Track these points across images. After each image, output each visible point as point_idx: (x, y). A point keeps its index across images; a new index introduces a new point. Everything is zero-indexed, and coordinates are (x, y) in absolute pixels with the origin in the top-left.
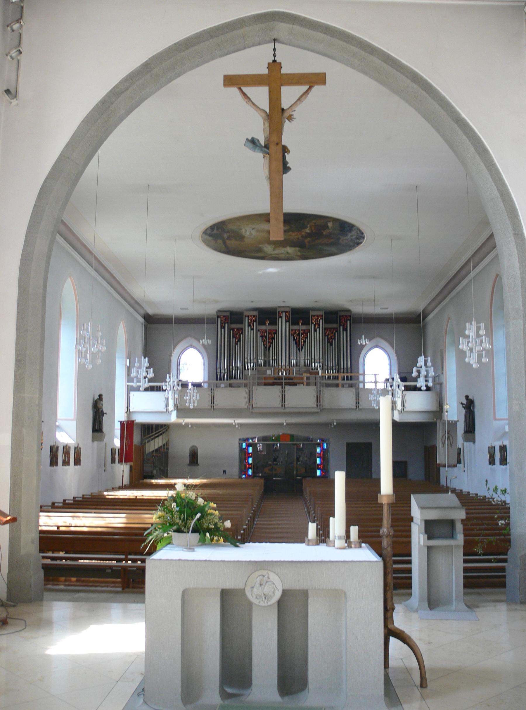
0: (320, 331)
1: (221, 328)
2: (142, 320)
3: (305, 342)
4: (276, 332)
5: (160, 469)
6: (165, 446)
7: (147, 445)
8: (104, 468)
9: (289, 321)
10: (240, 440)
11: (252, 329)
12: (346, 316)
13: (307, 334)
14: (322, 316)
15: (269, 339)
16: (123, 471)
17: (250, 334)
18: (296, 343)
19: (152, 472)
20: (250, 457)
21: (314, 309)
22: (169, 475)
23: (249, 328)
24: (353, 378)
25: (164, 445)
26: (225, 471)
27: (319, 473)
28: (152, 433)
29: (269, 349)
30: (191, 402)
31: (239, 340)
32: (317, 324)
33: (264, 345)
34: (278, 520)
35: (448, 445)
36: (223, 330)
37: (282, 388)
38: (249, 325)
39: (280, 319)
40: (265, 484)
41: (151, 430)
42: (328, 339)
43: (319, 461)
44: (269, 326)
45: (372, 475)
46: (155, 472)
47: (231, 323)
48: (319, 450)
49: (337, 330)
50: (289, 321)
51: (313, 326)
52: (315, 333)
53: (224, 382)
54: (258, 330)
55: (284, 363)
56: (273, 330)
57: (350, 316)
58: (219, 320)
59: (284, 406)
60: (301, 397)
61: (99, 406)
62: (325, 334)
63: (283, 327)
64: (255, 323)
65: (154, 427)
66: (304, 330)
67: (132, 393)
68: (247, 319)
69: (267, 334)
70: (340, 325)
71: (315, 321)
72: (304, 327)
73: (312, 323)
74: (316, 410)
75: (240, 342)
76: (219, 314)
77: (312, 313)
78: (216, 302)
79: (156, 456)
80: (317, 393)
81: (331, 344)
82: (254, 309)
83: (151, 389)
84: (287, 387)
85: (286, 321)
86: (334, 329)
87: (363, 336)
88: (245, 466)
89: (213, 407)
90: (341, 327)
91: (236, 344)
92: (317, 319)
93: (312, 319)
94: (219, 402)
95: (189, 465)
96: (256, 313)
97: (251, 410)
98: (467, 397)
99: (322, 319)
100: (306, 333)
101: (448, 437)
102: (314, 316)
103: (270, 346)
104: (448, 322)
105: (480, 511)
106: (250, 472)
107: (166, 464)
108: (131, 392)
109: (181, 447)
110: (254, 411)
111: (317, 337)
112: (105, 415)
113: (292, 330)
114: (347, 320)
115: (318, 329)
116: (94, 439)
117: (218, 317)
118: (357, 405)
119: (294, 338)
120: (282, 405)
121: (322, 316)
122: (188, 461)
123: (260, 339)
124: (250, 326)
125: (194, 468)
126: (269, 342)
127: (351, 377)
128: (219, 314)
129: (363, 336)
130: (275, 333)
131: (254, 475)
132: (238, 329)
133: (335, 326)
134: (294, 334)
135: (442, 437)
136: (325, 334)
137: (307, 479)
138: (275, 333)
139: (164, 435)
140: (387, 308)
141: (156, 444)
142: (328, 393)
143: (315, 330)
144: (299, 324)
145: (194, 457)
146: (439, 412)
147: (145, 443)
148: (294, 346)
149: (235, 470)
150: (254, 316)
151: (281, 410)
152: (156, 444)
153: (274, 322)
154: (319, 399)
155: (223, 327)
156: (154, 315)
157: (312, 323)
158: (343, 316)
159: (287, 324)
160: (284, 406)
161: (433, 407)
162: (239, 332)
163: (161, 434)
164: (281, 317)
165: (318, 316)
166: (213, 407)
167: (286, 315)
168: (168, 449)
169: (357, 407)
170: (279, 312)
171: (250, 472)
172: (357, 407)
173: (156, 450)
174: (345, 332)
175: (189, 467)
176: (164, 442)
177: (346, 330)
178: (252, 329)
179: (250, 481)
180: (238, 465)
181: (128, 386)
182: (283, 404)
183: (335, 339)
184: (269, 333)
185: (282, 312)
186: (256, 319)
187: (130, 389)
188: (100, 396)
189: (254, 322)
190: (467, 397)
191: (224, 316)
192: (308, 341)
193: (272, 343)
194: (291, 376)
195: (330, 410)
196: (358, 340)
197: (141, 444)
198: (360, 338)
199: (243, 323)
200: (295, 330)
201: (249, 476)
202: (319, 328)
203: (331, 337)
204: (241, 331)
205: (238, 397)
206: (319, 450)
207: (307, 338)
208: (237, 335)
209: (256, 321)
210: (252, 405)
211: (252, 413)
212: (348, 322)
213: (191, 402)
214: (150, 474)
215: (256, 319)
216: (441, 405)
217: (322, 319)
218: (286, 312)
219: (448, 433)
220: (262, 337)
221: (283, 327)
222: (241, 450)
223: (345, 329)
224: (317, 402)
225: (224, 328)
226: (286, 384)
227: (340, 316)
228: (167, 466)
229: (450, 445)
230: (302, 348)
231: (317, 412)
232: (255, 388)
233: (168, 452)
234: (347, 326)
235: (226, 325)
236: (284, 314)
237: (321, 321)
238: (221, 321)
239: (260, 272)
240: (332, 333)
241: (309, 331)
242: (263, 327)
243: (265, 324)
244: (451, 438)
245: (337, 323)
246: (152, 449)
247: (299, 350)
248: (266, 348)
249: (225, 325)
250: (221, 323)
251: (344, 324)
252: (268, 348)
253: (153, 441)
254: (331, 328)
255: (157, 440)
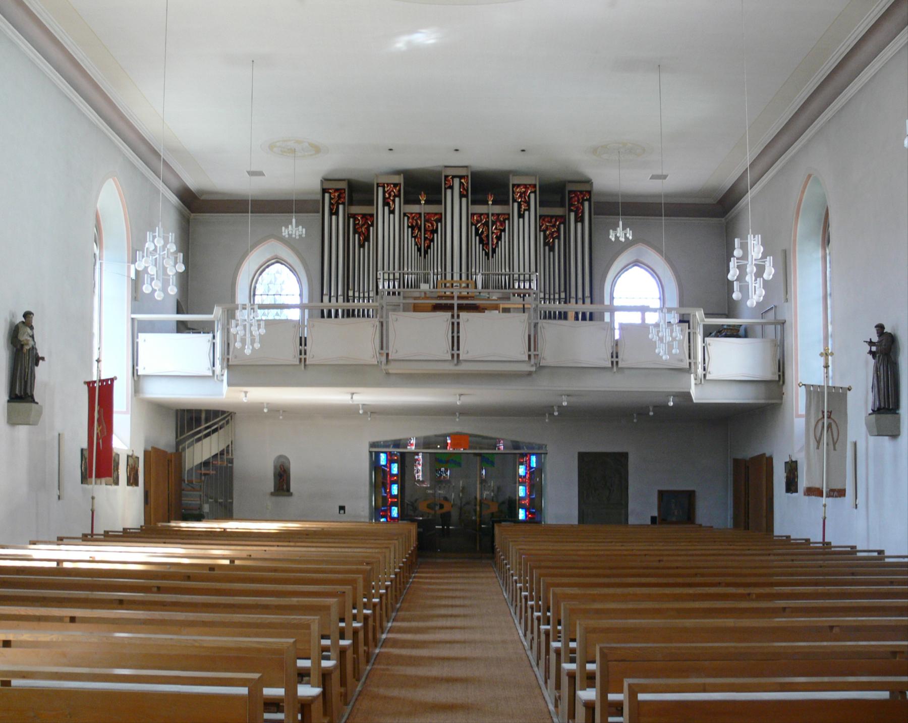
0: (531, 217)
1: (331, 214)
2: (174, 199)
3: (499, 238)
4: (440, 218)
5: (216, 502)
6: (225, 454)
7: (188, 453)
8: (56, 492)
9: (467, 196)
10: (373, 445)
11: (392, 212)
12: (581, 192)
13: (503, 223)
14: (535, 186)
15: (426, 232)
16: (124, 502)
17: (389, 226)
18: (481, 241)
19: (200, 508)
20: (395, 482)
21: (515, 173)
22: (234, 516)
23: (386, 208)
24: (595, 316)
25: (222, 453)
26: (342, 508)
27: (522, 514)
28: (200, 426)
29: (426, 252)
30: (248, 340)
31: (367, 239)
32: (525, 202)
33: (416, 244)
34: (456, 590)
35: (828, 444)
36: (334, 217)
37: (453, 316)
38: (386, 203)
39: (449, 192)
40: (420, 536)
41: (192, 421)
42: (545, 237)
43: (522, 491)
44: (426, 206)
45: (627, 520)
46: (206, 508)
47: (351, 203)
48: (522, 470)
49: (563, 219)
50: (467, 196)
51: (516, 205)
52: (521, 220)
53: (337, 320)
54: (405, 215)
55: (456, 277)
56: (436, 214)
57: (589, 192)
58: (327, 195)
59: (456, 358)
60: (495, 336)
61: (23, 337)
62: (540, 228)
63: (456, 210)
64: (397, 200)
65: (203, 416)
66: (498, 215)
67: (142, 337)
68: (380, 189)
69: (422, 222)
70: (570, 211)
71: (520, 196)
72: (497, 209)
73: (514, 200)
74: (526, 368)
75: (369, 241)
76: (326, 186)
77: (514, 180)
78: (317, 149)
79: (205, 475)
80: (529, 330)
81: (552, 249)
82: (398, 172)
83: (183, 327)
84: (464, 315)
85: (462, 196)
86: (557, 217)
87: (621, 223)
88: (384, 499)
89: (303, 361)
90: (572, 215)
91: (362, 246)
92: (525, 193)
93: (513, 192)
94: (317, 352)
95: (272, 494)
96: (399, 179)
97: (384, 369)
98: (880, 328)
99: (535, 192)
100: (502, 220)
101: (829, 426)
102: (518, 186)
103: (429, 247)
104: (805, 188)
105: (820, 589)
106: (395, 512)
107: (228, 492)
108: (140, 335)
109: (256, 458)
110: (393, 368)
111: (523, 234)
112: (41, 362)
113: (473, 215)
114: (584, 200)
115: (527, 213)
116: (13, 420)
117: (324, 191)
118: (615, 360)
119: (477, 230)
120: (453, 355)
121: (535, 186)
122: (270, 486)
123: (407, 232)
124: (388, 205)
125: (283, 500)
126: (426, 239)
127: (591, 314)
128: (327, 185)
129: (621, 223)
130: (440, 220)
131: (402, 516)
132: (364, 216)
133: (558, 211)
134: (478, 222)
135: (816, 426)
136: (540, 227)
137: (503, 523)
138: (440, 220)
139: (221, 431)
140: (665, 177)
141: (202, 451)
142: (551, 330)
143: (521, 216)
144: (488, 204)
145: (282, 480)
146: (776, 384)
147: (184, 449)
148: (477, 247)
149: (361, 506)
150: (395, 185)
151: (450, 367)
152: (202, 451)
153: (435, 196)
154: (532, 342)
155: (334, 212)
156: (203, 192)
157: (514, 200)
158: (575, 192)
159: (464, 200)
160: (456, 358)
161: (769, 374)
162: (366, 223)
163: (216, 430)
164: (451, 188)
165: (525, 186)
166: (303, 361)
167: (461, 183)
168: (231, 461)
169: (615, 364)
170: (446, 177)
171: (395, 512)
172: (615, 364)
173: (206, 464)
174: (579, 225)
175: (274, 498)
176: (223, 447)
177: (582, 221)
178: (392, 212)
179: (393, 526)
180: (367, 494)
181: (133, 319)
182: (455, 352)
183: (558, 237)
184: (426, 221)
185: (453, 177)
186: (399, 191)
187: (138, 328)
188: (27, 315)
189: (395, 196)
190: (880, 328)
191: (336, 190)
192: (505, 237)
193: (432, 240)
194: (471, 290)
195: (556, 370)
196: (611, 231)
197: (177, 449)
198: (615, 227)
199: (373, 205)
200: (480, 215)
201: (393, 519)
202: (529, 210)
203: (551, 232)
204: (369, 220)
205: (356, 339)
206: (522, 470)
207: (504, 230)
208: (363, 228)
209: (399, 196)
210: (387, 355)
211: (388, 374)
212: (586, 204)
213: (248, 340)
214: (197, 512)
215: (399, 191)
216: (781, 367)
217: (535, 192)
218: (461, 177)
219: (829, 417)
220: (412, 227)
221: (456, 210)
222: (375, 465)
223: (580, 219)
224: (529, 350)
225: (337, 213)
226: (462, 308)
227: (570, 192)
228: (232, 498)
229: (831, 446)
230: (494, 251)
231: (530, 374)
232: (392, 316)
233: (232, 468)
234: (583, 212)
235: (341, 207)
236: (456, 182)
237: (532, 196)
238: (331, 199)
239: (400, 44)
240: (554, 226)
241: (507, 217)
242: (414, 209)
243: (419, 202)
244: (834, 426)
245: (562, 205)
246: (198, 460)
247: (487, 254)
248: (419, 250)
249: (338, 207)
250: (331, 204)
251: (578, 208)
252: (424, 251)
253: (199, 444)
254: (552, 217)
255: (206, 441)
